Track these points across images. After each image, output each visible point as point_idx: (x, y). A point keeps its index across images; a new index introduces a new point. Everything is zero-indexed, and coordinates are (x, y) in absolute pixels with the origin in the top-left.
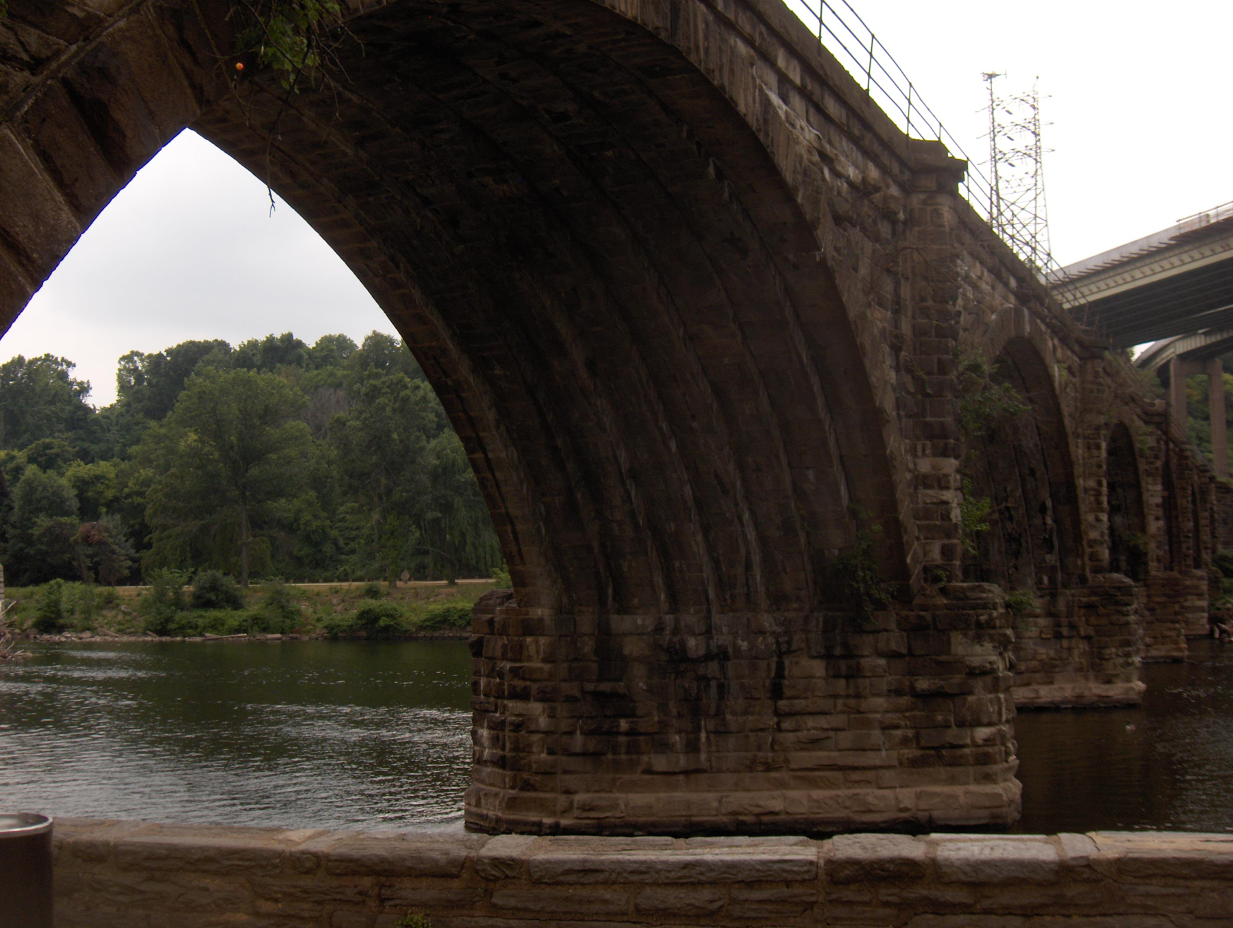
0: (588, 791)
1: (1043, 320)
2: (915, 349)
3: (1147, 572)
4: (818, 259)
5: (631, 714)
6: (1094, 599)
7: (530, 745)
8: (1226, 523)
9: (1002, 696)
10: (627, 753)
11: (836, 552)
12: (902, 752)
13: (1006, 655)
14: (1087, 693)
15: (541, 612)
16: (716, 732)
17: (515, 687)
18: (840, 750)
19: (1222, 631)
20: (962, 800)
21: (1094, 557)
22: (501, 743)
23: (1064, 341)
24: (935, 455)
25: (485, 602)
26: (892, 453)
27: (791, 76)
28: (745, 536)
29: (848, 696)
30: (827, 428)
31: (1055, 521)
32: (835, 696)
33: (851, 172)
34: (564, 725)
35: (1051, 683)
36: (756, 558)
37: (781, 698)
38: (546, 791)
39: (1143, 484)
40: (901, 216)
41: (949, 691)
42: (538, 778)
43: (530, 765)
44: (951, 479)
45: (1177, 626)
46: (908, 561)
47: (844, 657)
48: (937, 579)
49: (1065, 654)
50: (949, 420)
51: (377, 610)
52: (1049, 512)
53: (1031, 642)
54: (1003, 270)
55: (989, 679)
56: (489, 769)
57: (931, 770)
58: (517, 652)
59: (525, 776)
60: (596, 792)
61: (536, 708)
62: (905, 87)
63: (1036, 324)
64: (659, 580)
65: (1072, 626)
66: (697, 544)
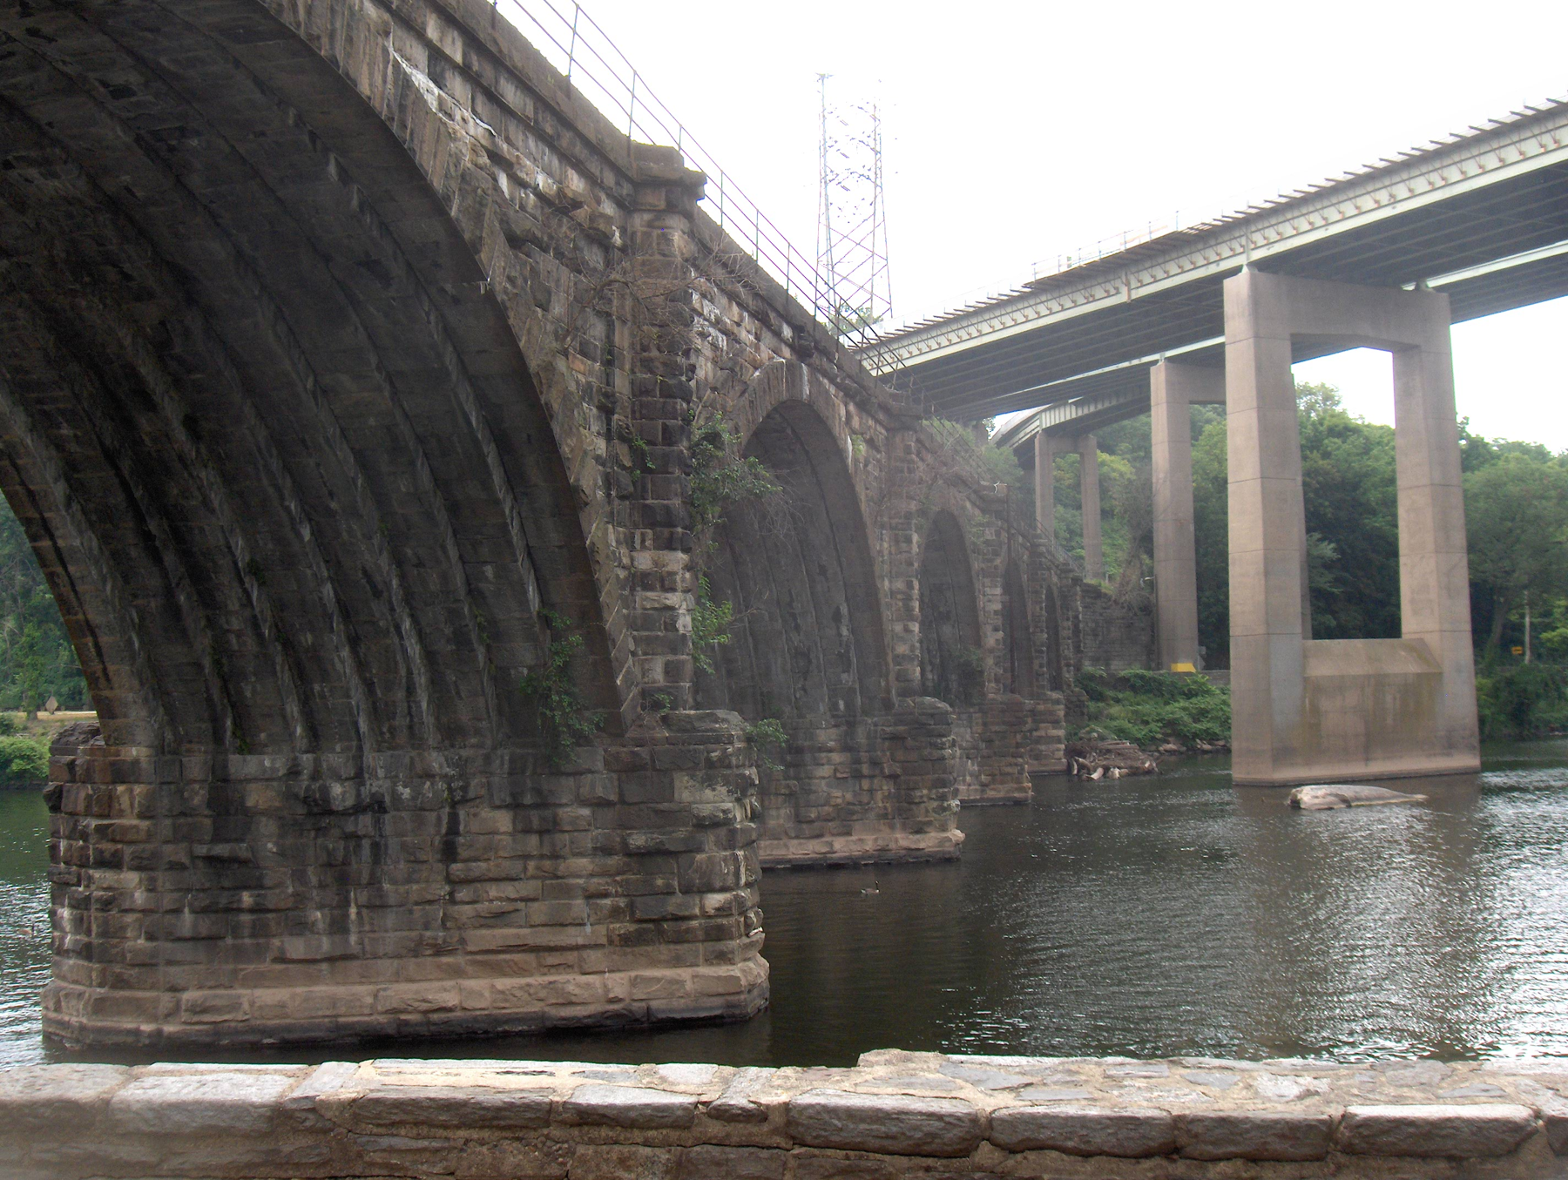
0: (201, 988)
1: (832, 381)
2: (633, 412)
3: (983, 695)
4: (482, 292)
5: (257, 885)
6: (901, 728)
7: (123, 928)
8: (1096, 635)
9: (740, 853)
10: (253, 936)
11: (525, 671)
12: (611, 926)
13: (747, 801)
14: (892, 846)
15: (136, 752)
16: (370, 907)
17: (102, 852)
18: (532, 926)
19: (1082, 767)
20: (689, 986)
21: (902, 677)
22: (85, 926)
23: (863, 406)
24: (657, 547)
25: (65, 740)
26: (593, 544)
27: (448, 51)
28: (404, 651)
29: (542, 857)
30: (507, 511)
31: (853, 631)
32: (526, 857)
33: (541, 180)
34: (168, 901)
35: (849, 834)
36: (421, 680)
37: (455, 861)
38: (145, 989)
39: (978, 586)
40: (617, 239)
41: (672, 849)
42: (134, 972)
43: (123, 955)
44: (678, 578)
45: (1020, 760)
46: (618, 682)
47: (536, 806)
48: (657, 705)
49: (865, 799)
50: (676, 502)
51: (8, 750)
52: (845, 621)
53: (823, 782)
54: (772, 315)
55: (722, 832)
56: (71, 962)
57: (649, 949)
58: (107, 806)
59: (117, 969)
60: (211, 988)
61: (131, 878)
62: (627, 77)
63: (820, 384)
64: (293, 709)
65: (875, 763)
66: (343, 660)
